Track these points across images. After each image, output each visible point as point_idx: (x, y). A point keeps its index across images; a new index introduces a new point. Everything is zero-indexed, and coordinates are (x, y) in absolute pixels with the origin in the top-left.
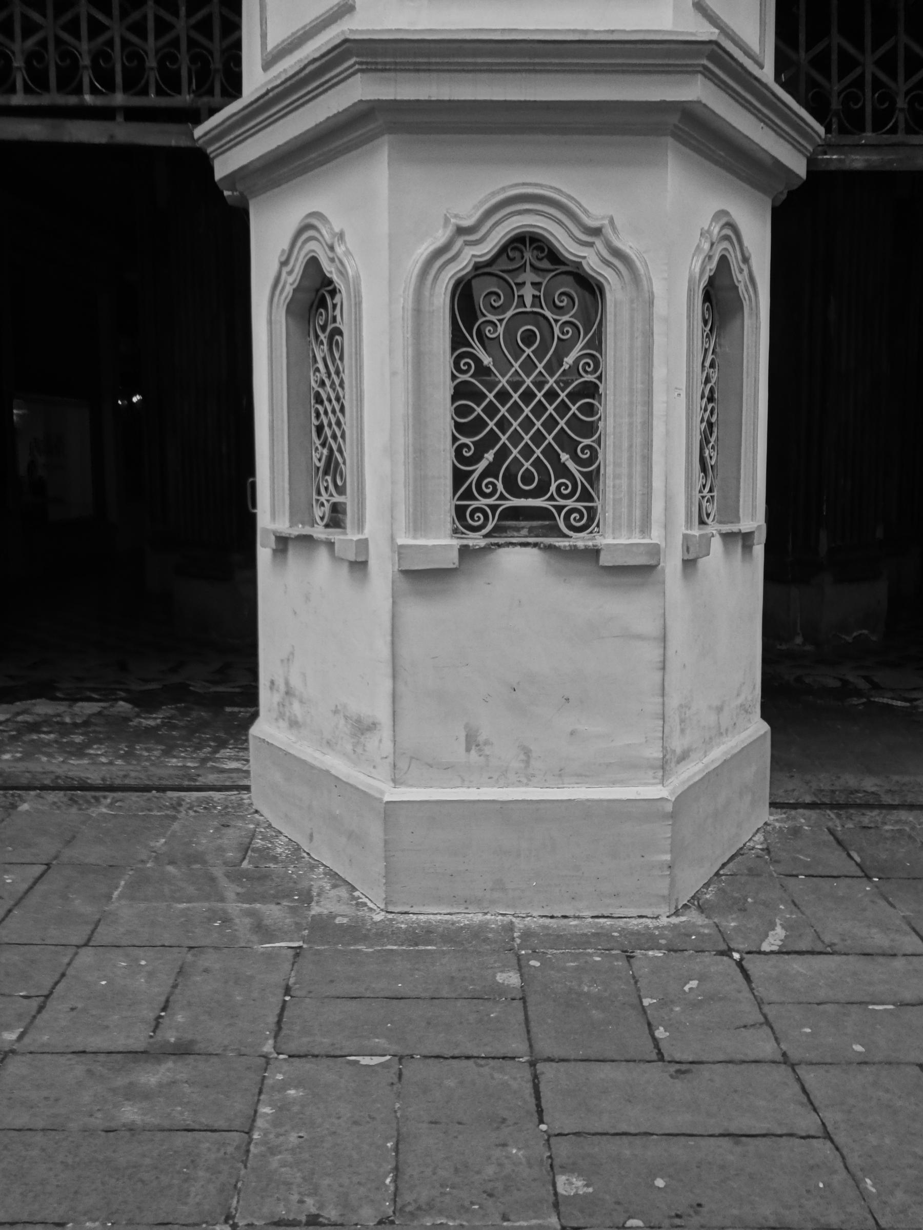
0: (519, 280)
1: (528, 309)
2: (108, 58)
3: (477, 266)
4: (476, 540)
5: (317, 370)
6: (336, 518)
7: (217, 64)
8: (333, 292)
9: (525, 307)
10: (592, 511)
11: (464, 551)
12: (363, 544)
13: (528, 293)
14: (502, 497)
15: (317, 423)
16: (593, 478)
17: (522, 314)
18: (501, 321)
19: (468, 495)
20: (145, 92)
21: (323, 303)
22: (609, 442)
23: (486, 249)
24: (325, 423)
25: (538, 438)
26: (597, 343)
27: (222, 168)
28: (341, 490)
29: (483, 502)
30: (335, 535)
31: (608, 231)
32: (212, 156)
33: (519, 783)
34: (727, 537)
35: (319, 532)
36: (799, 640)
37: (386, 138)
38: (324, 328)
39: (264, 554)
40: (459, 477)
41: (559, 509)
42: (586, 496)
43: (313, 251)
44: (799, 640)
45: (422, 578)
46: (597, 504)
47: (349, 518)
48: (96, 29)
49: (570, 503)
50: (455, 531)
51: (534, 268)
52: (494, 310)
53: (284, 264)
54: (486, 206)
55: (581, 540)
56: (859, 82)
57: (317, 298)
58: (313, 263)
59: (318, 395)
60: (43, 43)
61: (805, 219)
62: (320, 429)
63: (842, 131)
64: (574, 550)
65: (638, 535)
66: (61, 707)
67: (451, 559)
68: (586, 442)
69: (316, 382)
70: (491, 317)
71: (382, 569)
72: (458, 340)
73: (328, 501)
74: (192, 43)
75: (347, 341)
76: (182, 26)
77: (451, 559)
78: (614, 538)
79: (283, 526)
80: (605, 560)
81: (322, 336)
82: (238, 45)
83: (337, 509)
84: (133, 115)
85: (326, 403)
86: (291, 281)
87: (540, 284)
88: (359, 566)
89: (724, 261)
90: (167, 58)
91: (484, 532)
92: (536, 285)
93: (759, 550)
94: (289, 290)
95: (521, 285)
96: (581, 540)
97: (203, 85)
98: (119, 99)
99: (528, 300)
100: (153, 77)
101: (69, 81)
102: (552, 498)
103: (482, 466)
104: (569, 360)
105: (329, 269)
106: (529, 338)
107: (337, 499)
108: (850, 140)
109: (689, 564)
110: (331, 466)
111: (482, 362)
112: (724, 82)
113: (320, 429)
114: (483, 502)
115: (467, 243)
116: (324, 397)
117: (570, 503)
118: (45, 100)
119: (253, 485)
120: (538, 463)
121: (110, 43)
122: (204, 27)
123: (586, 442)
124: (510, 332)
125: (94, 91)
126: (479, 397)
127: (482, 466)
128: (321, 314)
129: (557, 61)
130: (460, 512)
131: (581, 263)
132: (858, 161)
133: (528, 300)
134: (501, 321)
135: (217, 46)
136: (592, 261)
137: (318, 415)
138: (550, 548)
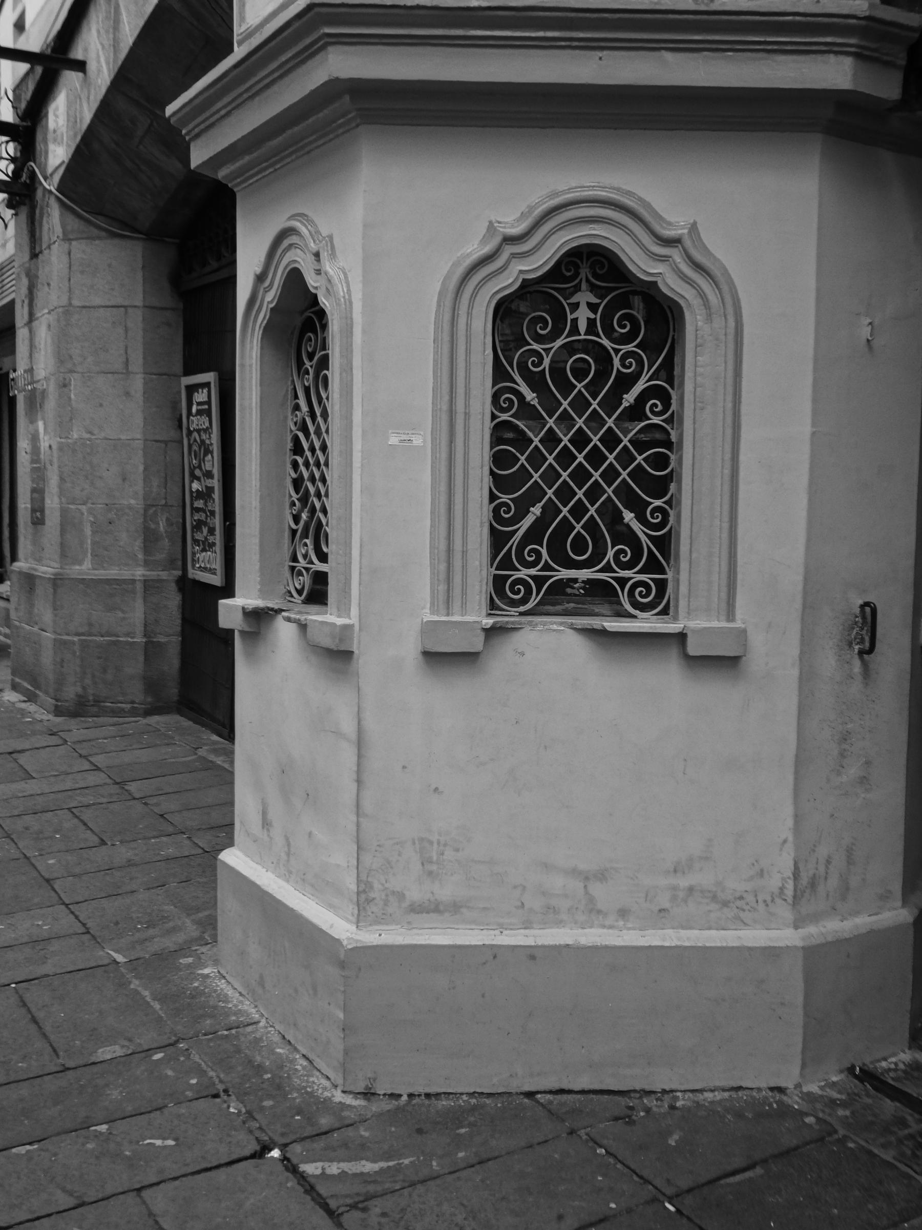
0: (573, 300)
1: (582, 337)
3: (526, 284)
4: (510, 616)
5: (297, 407)
9: (580, 335)
10: (662, 585)
14: (547, 567)
15: (294, 475)
16: (665, 544)
18: (547, 351)
19: (506, 564)
23: (539, 262)
24: (306, 475)
25: (594, 493)
29: (524, 573)
31: (688, 243)
32: (187, 138)
33: (544, 924)
37: (848, 61)
38: (311, 356)
40: (498, 539)
41: (622, 582)
42: (653, 566)
43: (295, 261)
46: (670, 575)
50: (492, 605)
51: (593, 288)
52: (539, 339)
54: (603, 194)
58: (295, 277)
59: (296, 440)
65: (723, 618)
68: (658, 503)
69: (296, 424)
70: (536, 346)
72: (499, 373)
73: (307, 569)
75: (334, 373)
81: (308, 364)
83: (321, 579)
85: (308, 453)
86: (270, 297)
87: (598, 305)
91: (522, 609)
92: (593, 307)
95: (575, 307)
99: (582, 326)
102: (608, 569)
103: (527, 522)
106: (580, 373)
107: (319, 566)
111: (525, 398)
112: (282, 130)
114: (524, 573)
115: (514, 256)
116: (306, 445)
120: (591, 526)
123: (658, 503)
126: (522, 441)
127: (527, 522)
128: (310, 340)
129: (289, 54)
130: (499, 583)
131: (655, 283)
133: (582, 326)
134: (547, 351)
137: (295, 465)
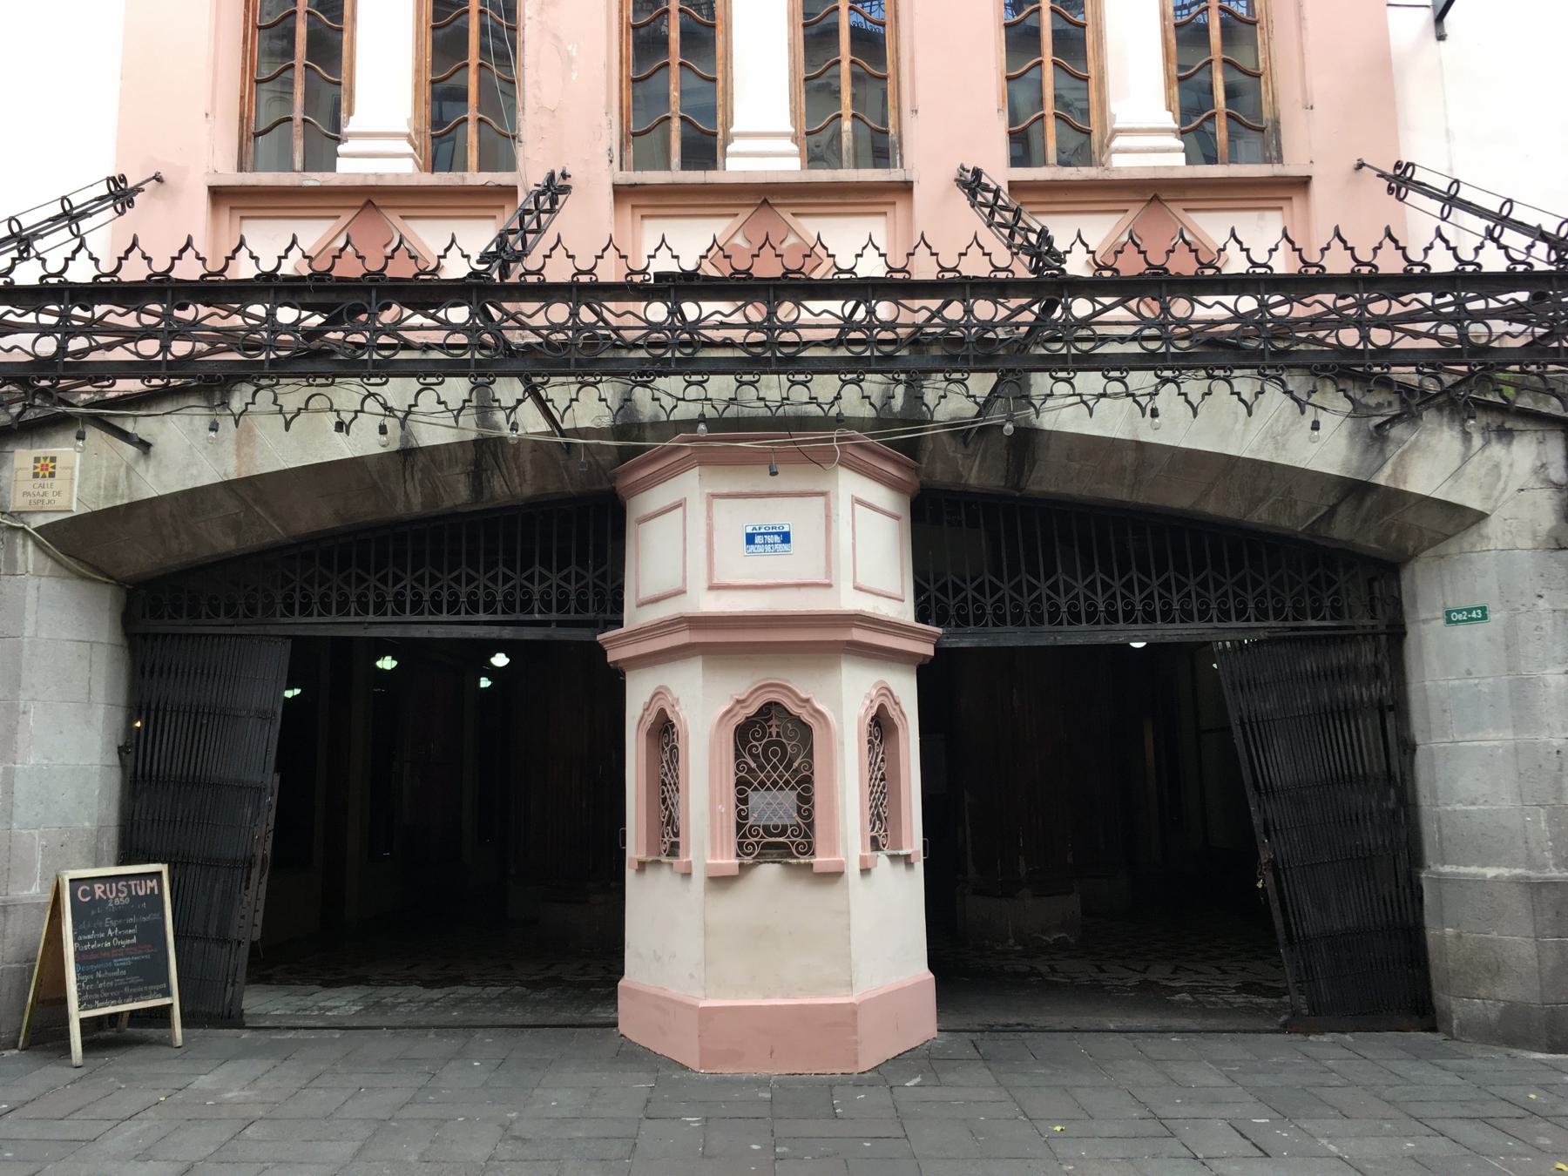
2: (549, 594)
4: (748, 860)
6: (674, 850)
7: (609, 597)
8: (673, 726)
10: (810, 845)
11: (741, 865)
12: (689, 863)
13: (774, 730)
17: (773, 745)
19: (744, 836)
20: (568, 612)
21: (666, 730)
22: (817, 806)
26: (810, 755)
27: (612, 656)
28: (676, 835)
30: (675, 861)
34: (893, 858)
35: (664, 859)
36: (1011, 942)
39: (630, 873)
42: (806, 836)
44: (1011, 942)
45: (720, 882)
47: (681, 852)
48: (543, 579)
49: (798, 840)
53: (646, 710)
55: (803, 860)
56: (965, 599)
57: (663, 730)
58: (662, 712)
60: (513, 588)
61: (935, 679)
62: (664, 800)
63: (957, 626)
64: (799, 865)
66: (478, 990)
67: (736, 871)
71: (699, 876)
74: (595, 585)
76: (590, 577)
77: (736, 871)
78: (820, 860)
79: (643, 856)
80: (816, 869)
82: (622, 587)
84: (560, 624)
86: (650, 718)
88: (687, 875)
89: (882, 707)
90: (581, 594)
93: (919, 866)
94: (648, 725)
96: (803, 860)
97: (601, 606)
98: (554, 616)
100: (573, 604)
101: (526, 606)
104: (796, 765)
105: (670, 715)
106: (775, 753)
108: (961, 630)
109: (865, 871)
110: (671, 821)
113: (664, 800)
117: (798, 840)
118: (512, 617)
119: (624, 833)
121: (550, 586)
122: (603, 577)
124: (765, 750)
125: (540, 612)
130: (740, 845)
132: (966, 643)
135: (609, 587)
136: (806, 718)
138: (787, 864)
